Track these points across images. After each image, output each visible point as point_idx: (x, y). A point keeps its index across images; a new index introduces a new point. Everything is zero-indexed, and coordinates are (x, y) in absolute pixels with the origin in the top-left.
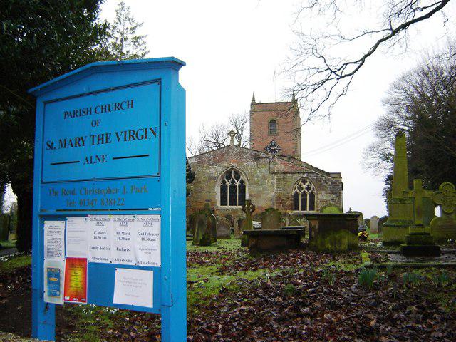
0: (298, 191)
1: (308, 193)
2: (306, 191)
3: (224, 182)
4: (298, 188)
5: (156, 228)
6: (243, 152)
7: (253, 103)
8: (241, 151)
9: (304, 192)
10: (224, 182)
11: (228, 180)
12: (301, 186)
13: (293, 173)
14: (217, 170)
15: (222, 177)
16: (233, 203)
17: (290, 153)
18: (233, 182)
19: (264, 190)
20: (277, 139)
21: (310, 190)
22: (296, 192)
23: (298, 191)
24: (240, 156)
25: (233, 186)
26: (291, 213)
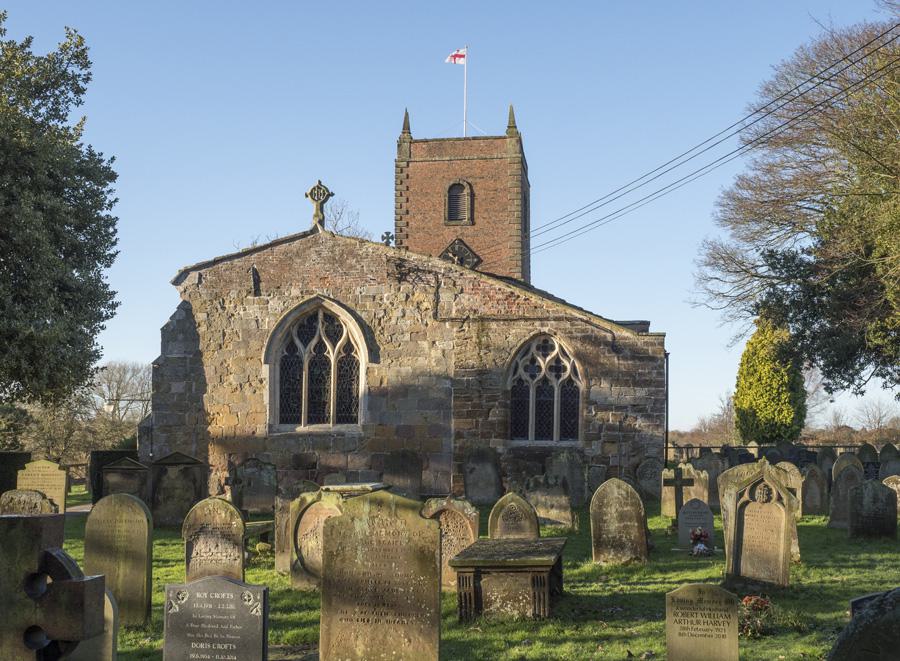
0: (525, 376)
1: (556, 385)
2: (551, 377)
3: (291, 348)
4: (526, 369)
5: (261, 430)
6: (352, 253)
7: (406, 142)
8: (347, 253)
9: (545, 380)
10: (291, 348)
11: (306, 343)
12: (533, 361)
13: (509, 320)
14: (269, 313)
15: (289, 334)
16: (317, 415)
17: (350, 500)
18: (321, 347)
19: (415, 343)
20: (468, 233)
21: (565, 375)
22: (520, 380)
23: (525, 376)
24: (342, 263)
25: (320, 363)
26: (499, 445)
